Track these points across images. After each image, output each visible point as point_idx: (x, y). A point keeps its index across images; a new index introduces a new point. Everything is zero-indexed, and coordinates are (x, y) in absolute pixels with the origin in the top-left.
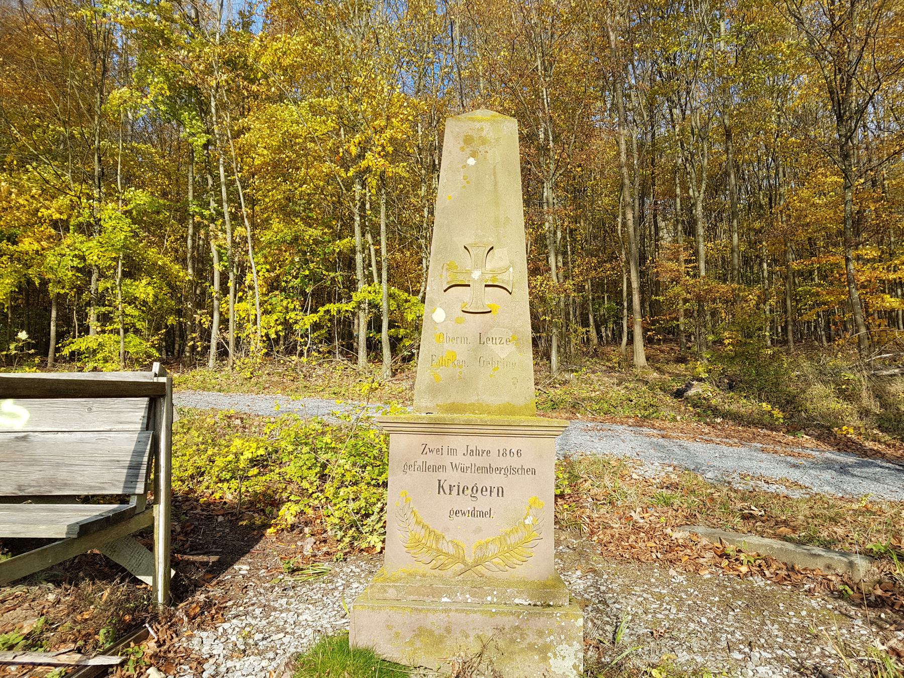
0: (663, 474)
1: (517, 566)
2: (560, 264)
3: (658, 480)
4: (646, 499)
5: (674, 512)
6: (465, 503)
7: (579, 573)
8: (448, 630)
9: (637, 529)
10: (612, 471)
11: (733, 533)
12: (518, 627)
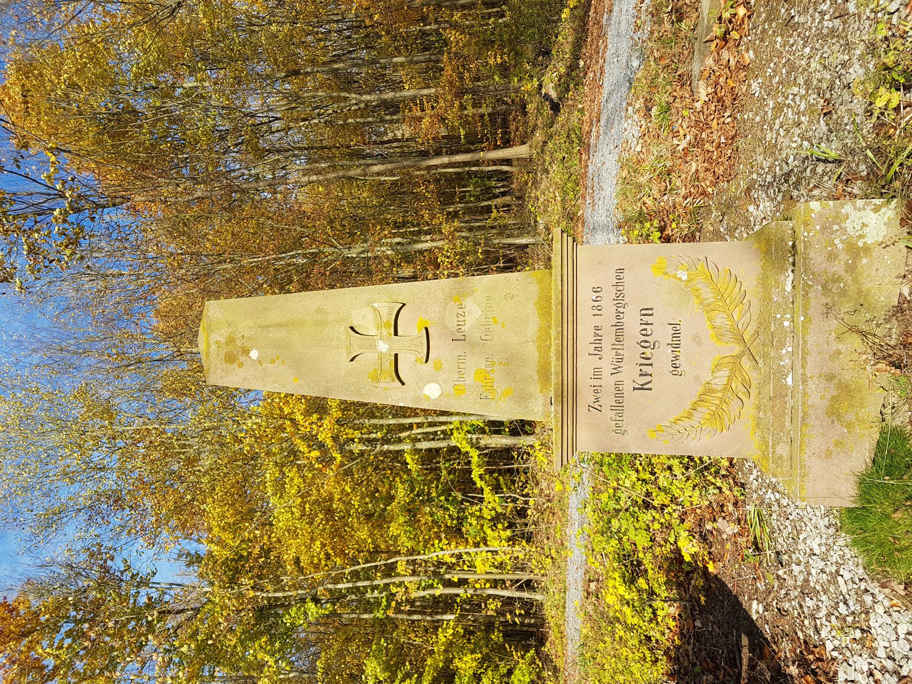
0: (635, 117)
1: (743, 289)
2: (428, 237)
3: (643, 122)
4: (663, 135)
5: (677, 100)
6: (662, 356)
7: (751, 208)
8: (830, 377)
9: (697, 143)
10: (633, 174)
11: (699, 30)
12: (824, 287)
